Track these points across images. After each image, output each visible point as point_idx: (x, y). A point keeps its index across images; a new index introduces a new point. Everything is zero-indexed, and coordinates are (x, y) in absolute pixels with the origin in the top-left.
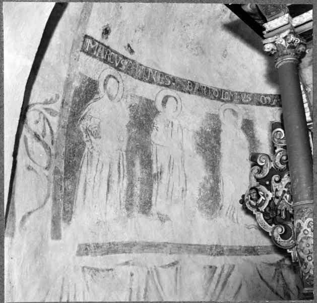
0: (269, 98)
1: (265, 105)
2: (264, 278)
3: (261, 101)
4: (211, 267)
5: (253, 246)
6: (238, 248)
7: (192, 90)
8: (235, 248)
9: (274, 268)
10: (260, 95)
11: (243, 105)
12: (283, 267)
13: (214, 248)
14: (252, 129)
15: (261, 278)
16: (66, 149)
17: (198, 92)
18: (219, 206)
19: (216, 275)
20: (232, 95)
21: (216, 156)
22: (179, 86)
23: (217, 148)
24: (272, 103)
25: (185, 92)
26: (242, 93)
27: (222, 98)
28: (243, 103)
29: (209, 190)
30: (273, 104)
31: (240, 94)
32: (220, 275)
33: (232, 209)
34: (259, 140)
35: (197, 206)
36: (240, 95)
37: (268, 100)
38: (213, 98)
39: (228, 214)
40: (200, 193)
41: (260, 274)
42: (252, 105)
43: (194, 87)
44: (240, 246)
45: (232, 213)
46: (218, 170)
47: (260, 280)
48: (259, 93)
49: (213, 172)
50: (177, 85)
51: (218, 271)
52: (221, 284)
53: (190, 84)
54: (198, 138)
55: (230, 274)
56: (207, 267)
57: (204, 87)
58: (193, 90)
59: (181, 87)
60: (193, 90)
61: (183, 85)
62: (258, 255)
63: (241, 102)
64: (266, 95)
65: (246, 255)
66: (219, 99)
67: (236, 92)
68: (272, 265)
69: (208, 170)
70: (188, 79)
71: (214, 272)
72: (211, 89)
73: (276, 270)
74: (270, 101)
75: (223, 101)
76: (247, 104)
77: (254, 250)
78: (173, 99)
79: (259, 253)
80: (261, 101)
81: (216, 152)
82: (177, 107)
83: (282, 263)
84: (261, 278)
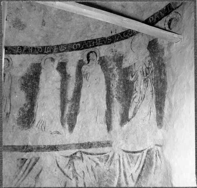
0: (79, 45)
1: (75, 50)
2: (60, 166)
3: (74, 48)
4: (23, 159)
5: (54, 145)
6: (43, 147)
7: (21, 51)
8: (41, 147)
9: (68, 159)
10: (73, 44)
11: (60, 53)
12: (75, 159)
13: (26, 147)
14: (65, 68)
15: (58, 165)
16: (139, 67)
17: (25, 52)
18: (32, 121)
19: (26, 165)
20: (52, 49)
21: (35, 90)
22: (10, 51)
23: (37, 85)
24: (81, 47)
25: (15, 54)
26: (60, 45)
27: (45, 52)
28: (60, 52)
29: (27, 112)
30: (82, 48)
31: (58, 46)
32: (28, 164)
33: (41, 122)
34: (69, 75)
35: (17, 122)
36: (58, 47)
37: (78, 46)
38: (37, 53)
39: (38, 126)
40: (20, 114)
41: (57, 163)
42: (66, 52)
43: (23, 50)
44: (44, 146)
45: (41, 125)
46: (35, 99)
47: (57, 167)
48: (71, 43)
49: (32, 100)
50: (9, 51)
51: (27, 162)
52: (28, 169)
53: (19, 48)
54: (23, 81)
55: (35, 164)
56: (20, 159)
57: (31, 48)
58: (22, 52)
59: (12, 51)
60: (22, 52)
61: (13, 50)
62: (58, 150)
63: (59, 52)
64: (77, 43)
65: (49, 151)
66: (43, 53)
67: (55, 46)
68: (67, 157)
69: (28, 99)
70: (17, 46)
71: (25, 162)
72: (36, 48)
73: (69, 160)
74: (80, 46)
75: (45, 53)
76: (63, 52)
77: (55, 148)
78: (91, 54)
79: (59, 150)
80: (74, 48)
81: (35, 87)
82: (9, 64)
83: (75, 155)
84: (58, 165)
